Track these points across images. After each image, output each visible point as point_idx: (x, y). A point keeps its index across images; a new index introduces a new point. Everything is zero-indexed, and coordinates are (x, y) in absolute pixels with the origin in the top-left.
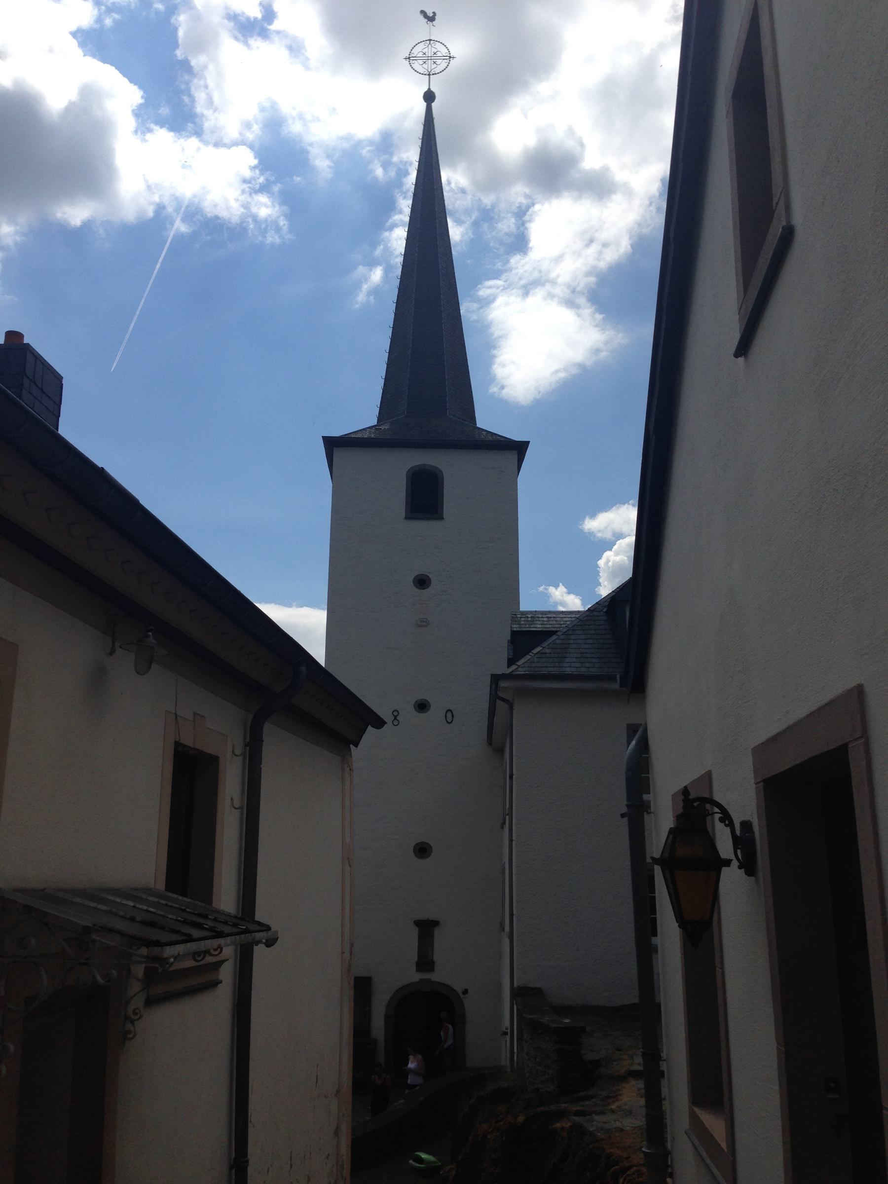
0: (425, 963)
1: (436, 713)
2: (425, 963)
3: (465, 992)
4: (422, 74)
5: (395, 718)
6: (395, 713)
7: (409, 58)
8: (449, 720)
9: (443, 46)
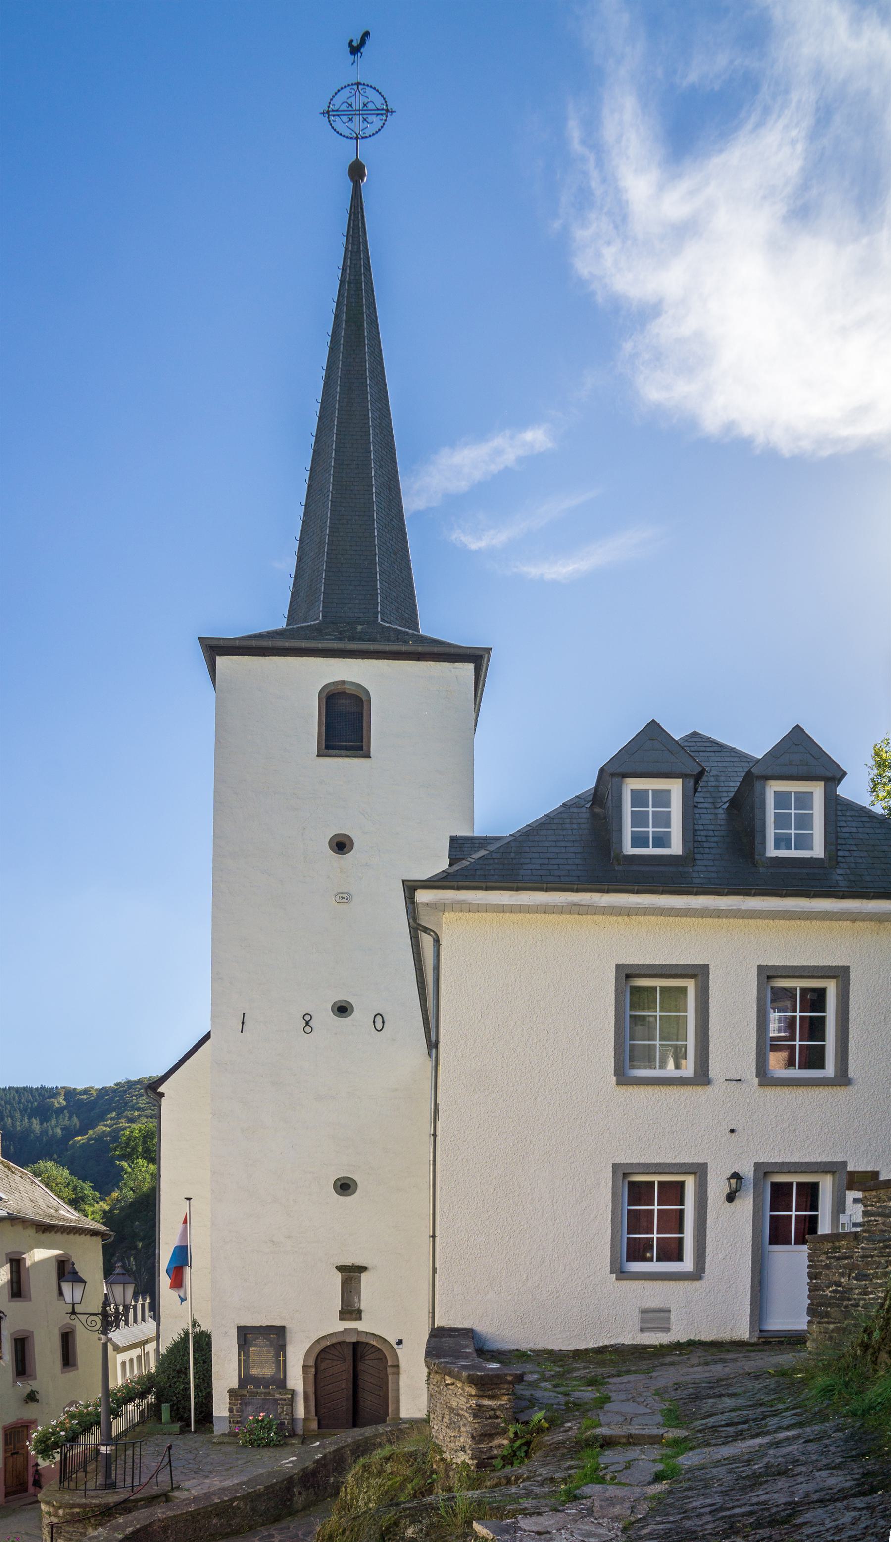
0: (350, 1311)
1: (361, 1016)
2: (350, 1311)
3: (400, 1342)
4: (348, 137)
5: (307, 1024)
6: (308, 1018)
7: (328, 112)
8: (379, 1019)
9: (378, 93)
